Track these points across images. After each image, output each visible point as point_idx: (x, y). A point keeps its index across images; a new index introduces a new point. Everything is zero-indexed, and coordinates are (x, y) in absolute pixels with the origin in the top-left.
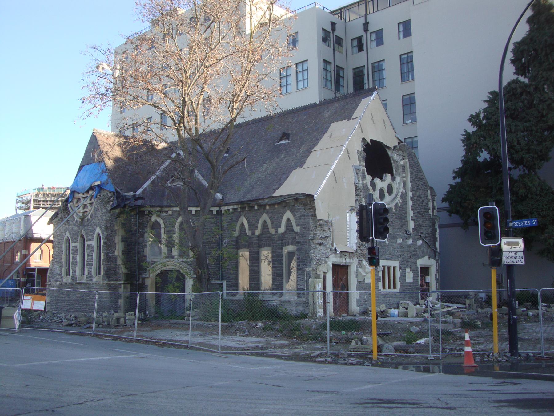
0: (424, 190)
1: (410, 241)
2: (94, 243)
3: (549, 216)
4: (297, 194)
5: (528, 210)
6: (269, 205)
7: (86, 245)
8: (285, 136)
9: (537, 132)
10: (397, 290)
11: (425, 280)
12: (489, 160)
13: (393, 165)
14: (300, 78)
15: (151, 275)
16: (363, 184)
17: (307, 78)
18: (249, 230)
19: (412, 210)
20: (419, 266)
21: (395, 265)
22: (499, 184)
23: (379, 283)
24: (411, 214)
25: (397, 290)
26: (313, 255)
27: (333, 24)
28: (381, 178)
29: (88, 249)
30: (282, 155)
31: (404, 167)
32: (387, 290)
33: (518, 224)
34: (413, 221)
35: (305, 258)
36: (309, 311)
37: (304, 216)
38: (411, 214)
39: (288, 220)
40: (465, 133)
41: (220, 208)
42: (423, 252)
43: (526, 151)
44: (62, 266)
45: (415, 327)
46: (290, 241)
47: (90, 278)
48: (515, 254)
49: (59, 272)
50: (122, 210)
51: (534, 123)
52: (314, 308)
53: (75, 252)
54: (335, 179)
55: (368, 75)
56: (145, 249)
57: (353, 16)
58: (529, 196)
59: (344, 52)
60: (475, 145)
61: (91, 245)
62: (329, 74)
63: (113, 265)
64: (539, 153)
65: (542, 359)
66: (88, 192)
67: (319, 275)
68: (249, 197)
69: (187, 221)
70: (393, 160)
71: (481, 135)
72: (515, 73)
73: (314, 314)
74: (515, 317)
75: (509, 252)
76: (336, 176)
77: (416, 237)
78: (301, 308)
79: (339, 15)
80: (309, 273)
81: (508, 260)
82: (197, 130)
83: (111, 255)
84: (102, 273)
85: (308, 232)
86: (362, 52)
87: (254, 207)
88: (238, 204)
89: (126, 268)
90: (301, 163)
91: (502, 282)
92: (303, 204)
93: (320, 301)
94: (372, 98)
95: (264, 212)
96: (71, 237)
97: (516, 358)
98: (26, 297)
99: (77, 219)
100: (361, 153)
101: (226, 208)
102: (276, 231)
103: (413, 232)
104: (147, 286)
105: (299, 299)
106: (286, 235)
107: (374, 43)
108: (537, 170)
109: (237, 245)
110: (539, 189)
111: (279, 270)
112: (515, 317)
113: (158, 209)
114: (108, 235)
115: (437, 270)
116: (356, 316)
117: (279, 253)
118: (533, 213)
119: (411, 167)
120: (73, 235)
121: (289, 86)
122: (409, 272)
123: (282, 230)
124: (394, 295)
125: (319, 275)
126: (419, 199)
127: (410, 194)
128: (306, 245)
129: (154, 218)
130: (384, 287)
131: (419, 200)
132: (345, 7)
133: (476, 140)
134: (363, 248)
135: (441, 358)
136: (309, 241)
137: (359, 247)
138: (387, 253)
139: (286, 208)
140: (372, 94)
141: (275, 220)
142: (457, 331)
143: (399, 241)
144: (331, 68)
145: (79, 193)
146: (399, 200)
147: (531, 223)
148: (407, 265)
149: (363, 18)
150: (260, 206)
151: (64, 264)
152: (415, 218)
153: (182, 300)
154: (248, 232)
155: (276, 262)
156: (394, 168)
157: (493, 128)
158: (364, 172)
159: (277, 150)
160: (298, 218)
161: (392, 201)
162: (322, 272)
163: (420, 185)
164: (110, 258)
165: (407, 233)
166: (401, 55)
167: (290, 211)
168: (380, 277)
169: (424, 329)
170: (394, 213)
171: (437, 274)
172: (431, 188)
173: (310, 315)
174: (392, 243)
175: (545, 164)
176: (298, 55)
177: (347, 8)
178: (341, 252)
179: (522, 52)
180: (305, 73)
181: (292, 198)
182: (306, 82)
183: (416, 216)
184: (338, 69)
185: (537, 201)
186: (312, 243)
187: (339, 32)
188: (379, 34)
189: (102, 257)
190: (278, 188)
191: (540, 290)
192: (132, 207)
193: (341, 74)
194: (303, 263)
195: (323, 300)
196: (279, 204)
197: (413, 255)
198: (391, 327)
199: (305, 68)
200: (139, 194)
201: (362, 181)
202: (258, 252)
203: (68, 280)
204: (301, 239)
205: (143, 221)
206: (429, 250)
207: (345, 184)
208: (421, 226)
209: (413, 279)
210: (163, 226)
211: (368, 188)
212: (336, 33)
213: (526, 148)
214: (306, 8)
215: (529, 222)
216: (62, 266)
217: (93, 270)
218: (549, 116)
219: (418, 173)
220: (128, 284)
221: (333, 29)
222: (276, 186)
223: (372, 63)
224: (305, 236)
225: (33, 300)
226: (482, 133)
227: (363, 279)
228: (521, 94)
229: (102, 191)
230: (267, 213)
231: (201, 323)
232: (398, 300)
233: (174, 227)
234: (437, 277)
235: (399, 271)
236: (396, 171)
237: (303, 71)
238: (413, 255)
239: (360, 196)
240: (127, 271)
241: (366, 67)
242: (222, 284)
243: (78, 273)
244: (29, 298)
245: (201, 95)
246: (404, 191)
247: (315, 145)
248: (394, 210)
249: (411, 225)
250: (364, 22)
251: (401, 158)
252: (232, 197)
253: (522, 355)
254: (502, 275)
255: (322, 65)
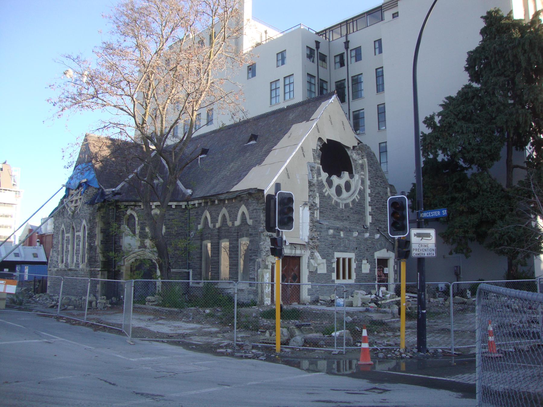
0: (383, 187)
1: (367, 235)
2: (81, 234)
3: (498, 211)
4: (250, 189)
5: (479, 206)
6: (228, 200)
7: (75, 236)
8: (254, 137)
9: (486, 133)
10: (352, 281)
11: (383, 271)
12: (446, 160)
13: (353, 163)
14: (287, 90)
15: (126, 263)
16: (318, 180)
17: (293, 90)
18: (212, 223)
19: (370, 205)
20: (376, 258)
21: (350, 257)
22: (454, 182)
23: (333, 273)
24: (369, 209)
25: (352, 281)
26: (263, 247)
27: (317, 43)
28: (339, 176)
29: (77, 239)
30: (248, 154)
31: (362, 166)
32: (341, 281)
33: (428, 215)
34: (371, 216)
35: (256, 249)
36: (258, 300)
37: (256, 209)
38: (369, 209)
39: (243, 213)
41: (188, 203)
42: (381, 245)
43: (477, 151)
44: (58, 254)
45: (349, 317)
47: (77, 265)
48: (425, 246)
49: (56, 260)
50: (103, 204)
51: (483, 125)
52: (262, 297)
53: (68, 243)
54: (288, 175)
55: (348, 87)
56: (121, 240)
57: (336, 36)
58: (481, 193)
59: (328, 68)
60: (430, 145)
61: (79, 235)
62: (313, 87)
63: (94, 254)
64: (489, 153)
65: (450, 355)
66: (78, 188)
67: (267, 265)
68: (212, 192)
69: (148, 213)
70: (353, 159)
71: (435, 136)
72: (469, 80)
73: (262, 302)
74: (424, 311)
75: (419, 244)
76: (289, 172)
77: (375, 231)
78: (252, 296)
79: (324, 35)
80: (259, 263)
81: (417, 252)
82: (162, 131)
83: (92, 244)
84: (86, 261)
86: (343, 67)
87: (214, 201)
88: (202, 199)
89: (104, 256)
90: (260, 161)
91: (460, 274)
92: (257, 199)
93: (268, 290)
94: (330, 101)
95: (223, 206)
96: (66, 229)
97: (422, 354)
99: (70, 212)
100: (316, 152)
101: (192, 203)
102: (233, 224)
103: (370, 226)
104: (122, 273)
105: (250, 288)
106: (242, 228)
107: (354, 59)
108: (488, 169)
109: (202, 237)
110: (489, 186)
111: (234, 260)
112: (424, 311)
113: (133, 203)
114: (91, 226)
115: (395, 262)
116: (306, 304)
117: (235, 244)
118: (484, 209)
119: (370, 165)
120: (67, 226)
121: (278, 98)
122: (366, 264)
124: (350, 285)
125: (267, 265)
126: (377, 195)
127: (368, 191)
129: (129, 212)
130: (338, 277)
131: (378, 197)
132: (329, 28)
133: (431, 141)
134: (316, 241)
135: (344, 353)
136: (260, 233)
137: (311, 239)
138: (342, 245)
139: (242, 202)
140: (331, 98)
141: (233, 213)
142: (394, 321)
143: (355, 234)
144: (315, 81)
145: (73, 190)
146: (357, 196)
147: (441, 213)
148: (363, 258)
149: (345, 38)
150: (220, 200)
151: (60, 253)
152: (373, 213)
154: (210, 225)
155: (234, 252)
156: (353, 166)
157: (446, 130)
158: (319, 169)
159: (244, 150)
160: (251, 212)
161: (350, 197)
162: (270, 262)
163: (380, 182)
164: (92, 247)
165: (364, 227)
166: (376, 69)
168: (334, 268)
169: (358, 319)
170: (351, 209)
171: (396, 266)
172: (391, 186)
173: (258, 303)
174: (348, 236)
175: (495, 163)
176: (285, 71)
177: (331, 29)
178: (291, 244)
179: (475, 60)
180: (292, 86)
181: (245, 193)
182: (292, 93)
183: (374, 212)
184: (322, 82)
185: (488, 197)
187: (323, 50)
188: (358, 50)
189: (86, 247)
190: (236, 184)
191: (452, 284)
193: (325, 87)
194: (254, 254)
195: (270, 288)
196: (235, 198)
197: (370, 248)
198: (328, 316)
199: (291, 81)
200: (118, 190)
201: (317, 177)
202: (219, 243)
203: (62, 266)
205: (120, 214)
206: (387, 243)
207: (298, 180)
208: (379, 221)
209: (370, 270)
210: (137, 219)
211: (323, 184)
212: (320, 51)
213: (477, 148)
214: (293, 29)
215: (439, 213)
216: (58, 254)
217: (79, 258)
218: (498, 118)
219: (377, 171)
220: (105, 270)
221: (318, 47)
222: (236, 182)
223: (352, 77)
224: (257, 229)
226: (436, 134)
227: (315, 269)
228: (473, 98)
229: (90, 188)
230: (226, 207)
231: (157, 308)
232: (353, 290)
234: (396, 269)
235: (355, 262)
237: (290, 84)
238: (370, 248)
239: (314, 191)
240: (104, 260)
241: (346, 80)
242: (189, 272)
243: (69, 261)
245: (168, 99)
246: (362, 188)
247: (276, 144)
248: (351, 206)
249: (369, 219)
250: (345, 41)
251: (360, 158)
252: (200, 193)
253: (430, 351)
254: (460, 267)
255: (307, 78)
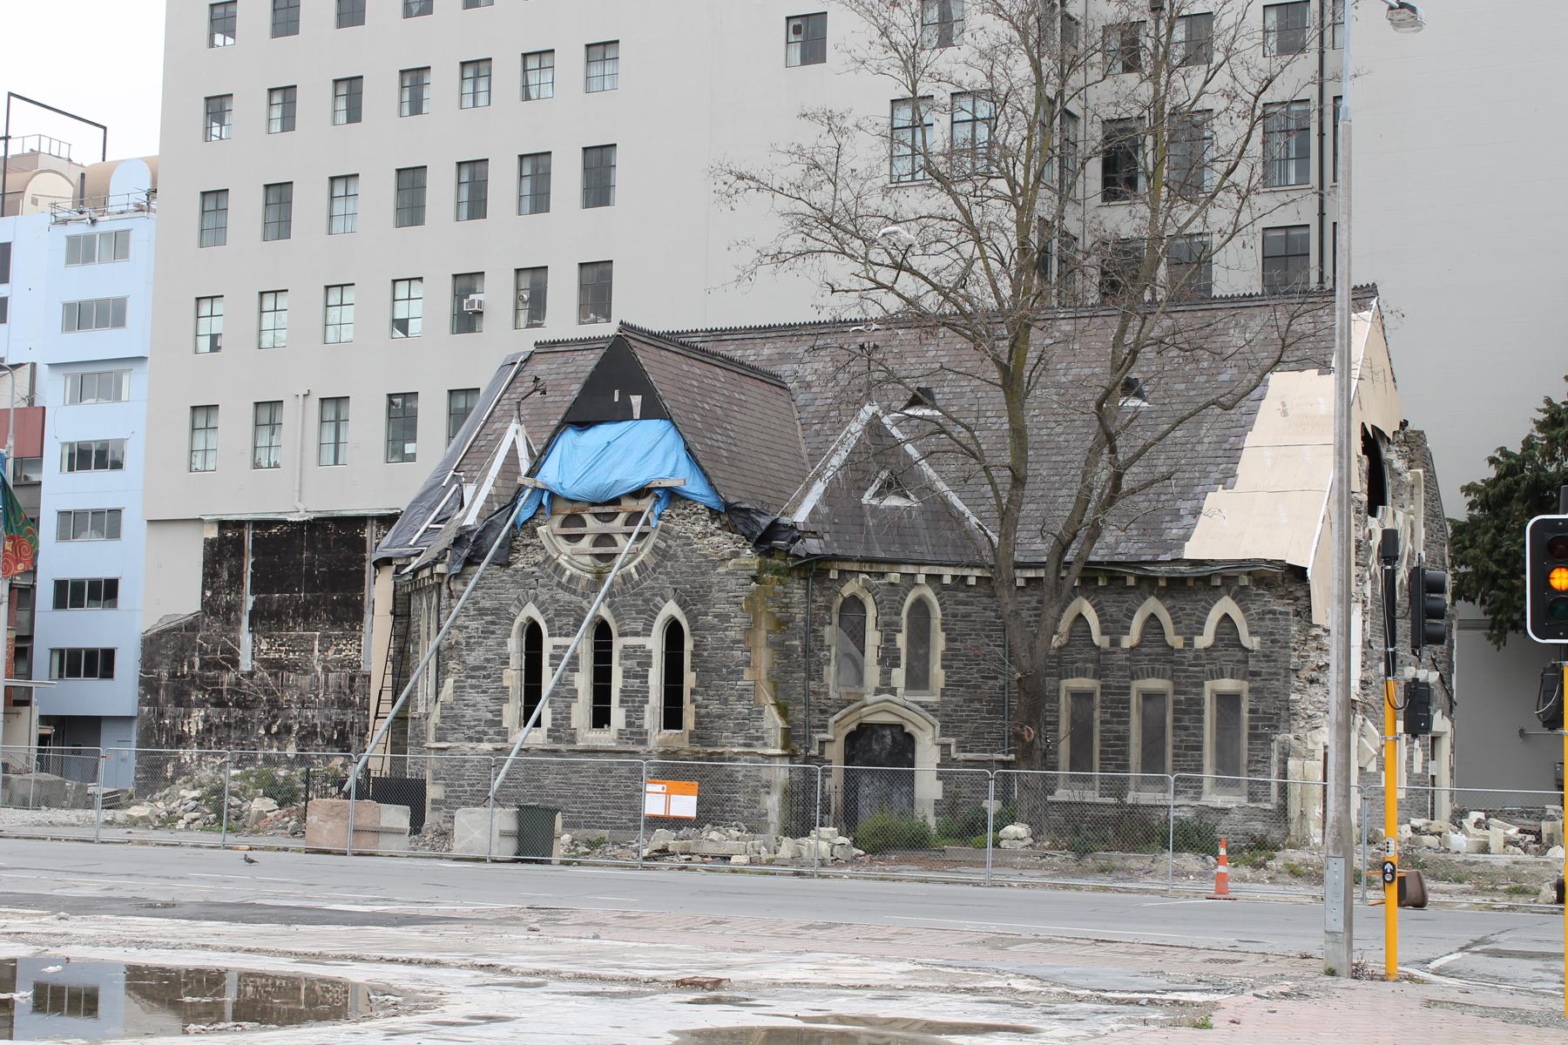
13: (1388, 480)
18: (1103, 633)
40: (1545, 406)
46: (1228, 668)
85: (1283, 651)
98: (650, 788)
102: (1189, 643)
123: (1204, 640)
128: (1278, 680)
153: (905, 800)
167: (1233, 598)
186: (1293, 677)
192: (800, 558)
204: (1264, 667)
225: (668, 793)
233: (898, 614)
236: (1393, 497)
244: (658, 788)
